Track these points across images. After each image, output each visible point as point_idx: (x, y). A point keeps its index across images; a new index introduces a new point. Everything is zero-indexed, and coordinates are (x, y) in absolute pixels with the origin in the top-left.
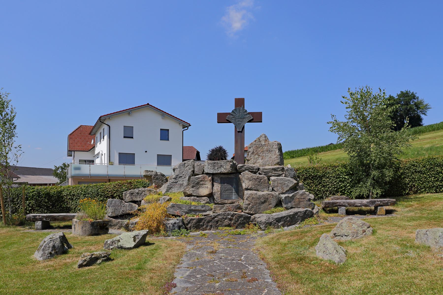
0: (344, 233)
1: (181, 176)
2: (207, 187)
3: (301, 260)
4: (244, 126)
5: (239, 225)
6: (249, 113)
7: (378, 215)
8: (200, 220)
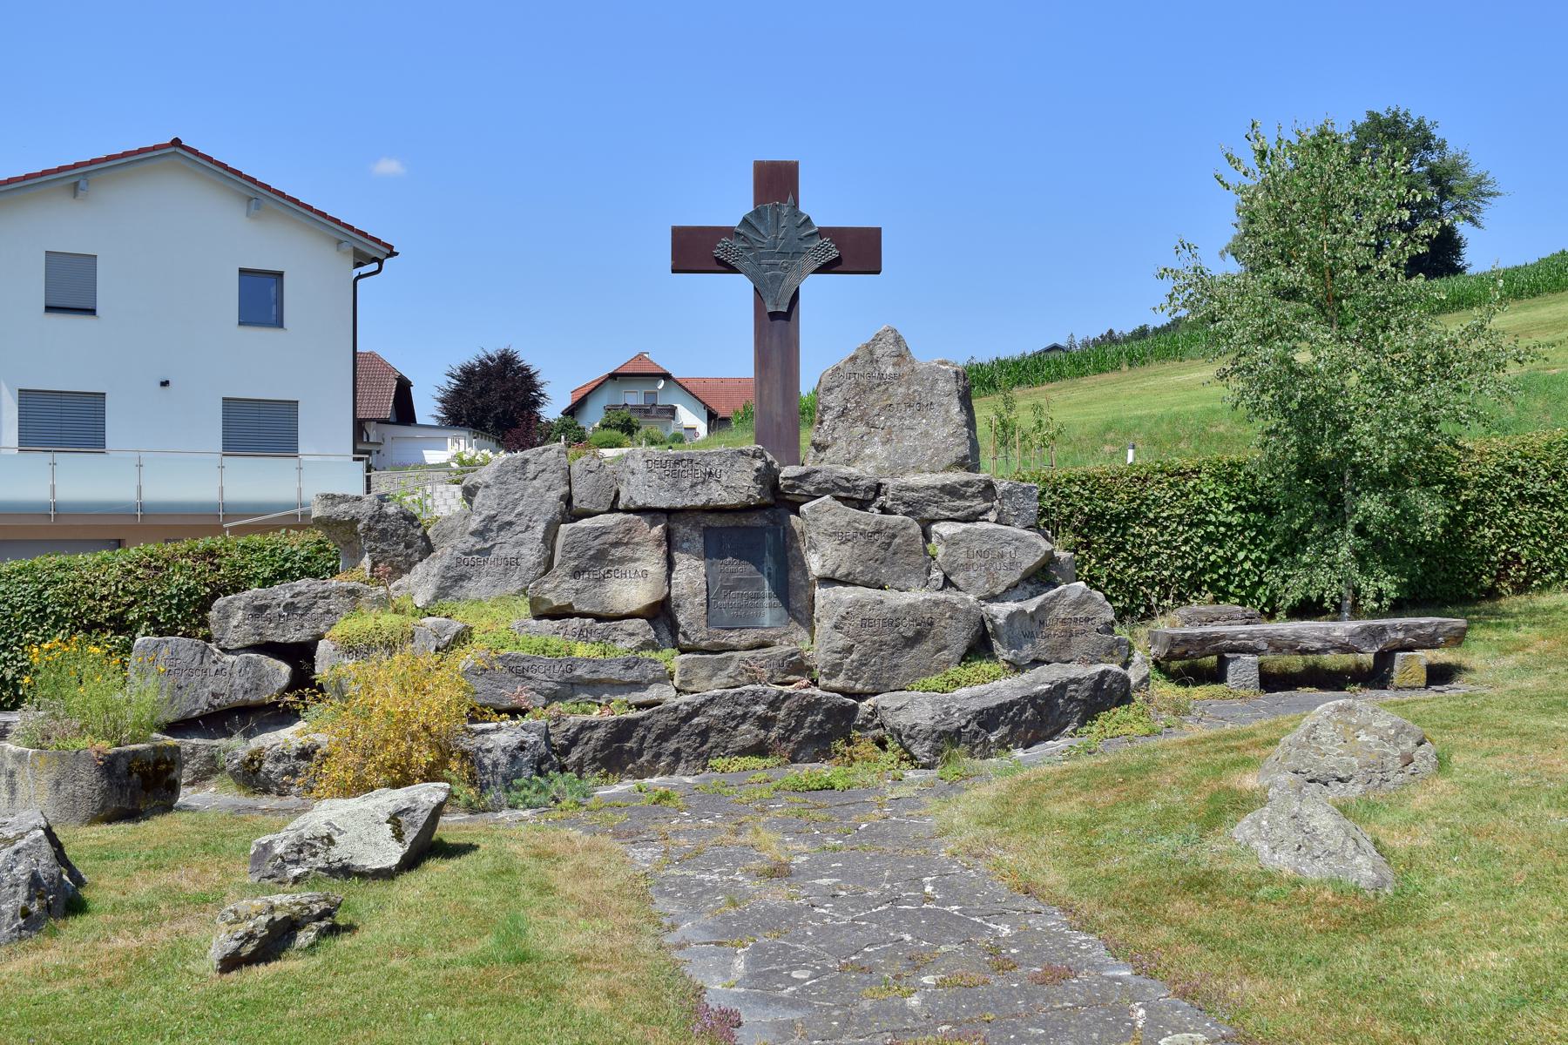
0: (1333, 769)
1: (510, 524)
2: (645, 574)
3: (1202, 884)
4: (798, 289)
5: (801, 745)
6: (822, 232)
7: (1398, 688)
8: (624, 729)
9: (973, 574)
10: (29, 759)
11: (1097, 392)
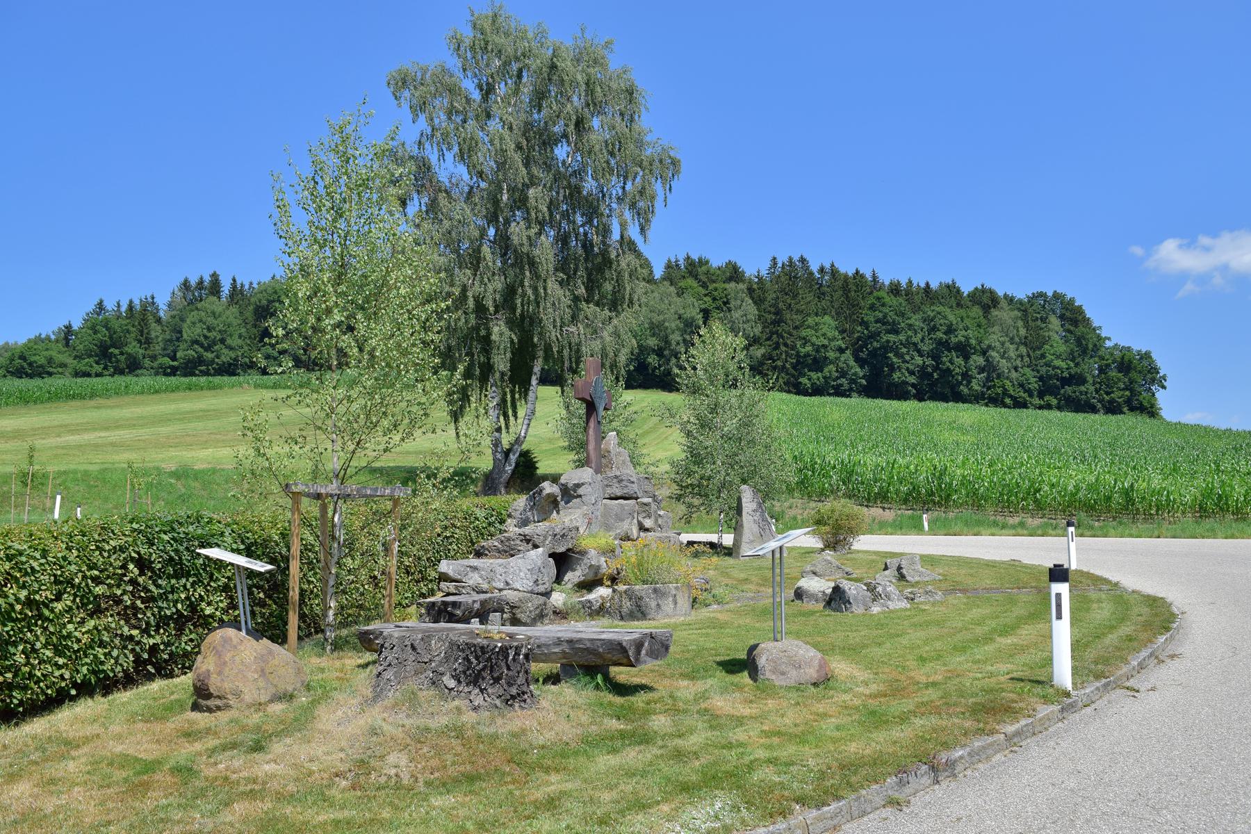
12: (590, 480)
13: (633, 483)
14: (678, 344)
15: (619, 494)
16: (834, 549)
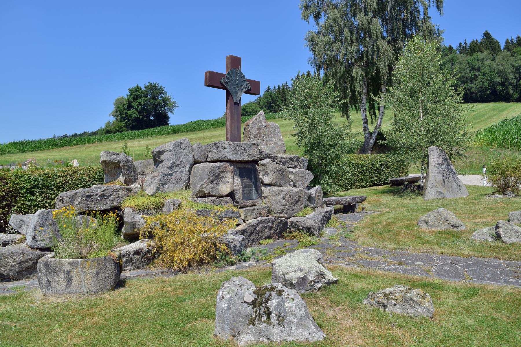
1: (179, 165)
9: (300, 183)
10: (80, 264)
11: (93, 149)
12: (170, 148)
13: (225, 148)
14: (512, 79)
15: (216, 158)
16: (504, 193)
